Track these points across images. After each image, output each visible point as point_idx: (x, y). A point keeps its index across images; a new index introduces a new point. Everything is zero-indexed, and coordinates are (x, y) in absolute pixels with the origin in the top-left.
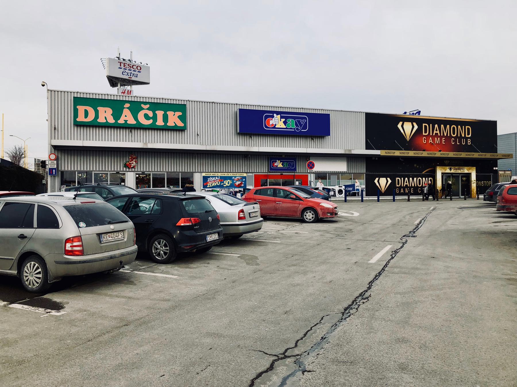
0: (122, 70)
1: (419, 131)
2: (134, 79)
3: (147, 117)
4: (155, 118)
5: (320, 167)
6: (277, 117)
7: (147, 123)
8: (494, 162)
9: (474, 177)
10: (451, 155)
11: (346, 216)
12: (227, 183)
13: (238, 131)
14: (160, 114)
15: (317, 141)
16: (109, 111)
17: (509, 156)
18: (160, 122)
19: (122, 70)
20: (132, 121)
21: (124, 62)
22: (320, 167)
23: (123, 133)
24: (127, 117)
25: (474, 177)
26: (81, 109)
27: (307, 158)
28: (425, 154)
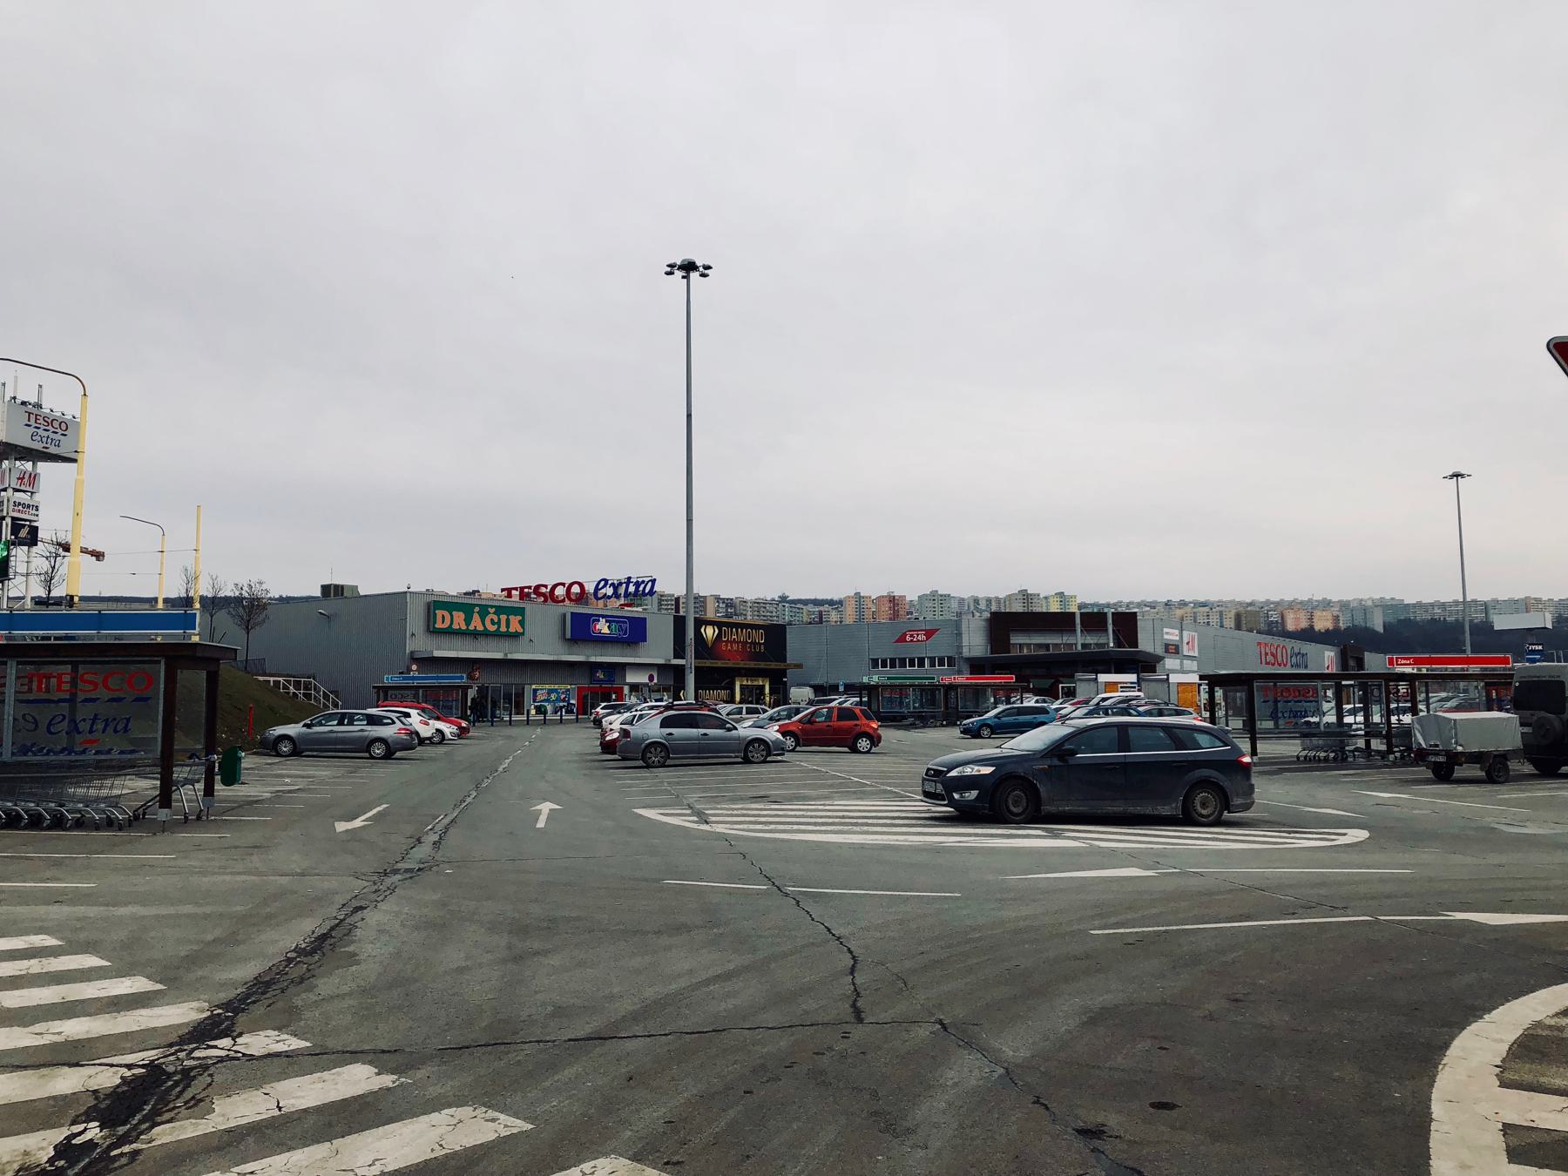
0: (32, 430)
1: (719, 635)
2: (53, 450)
3: (493, 622)
4: (499, 623)
5: (632, 678)
6: (603, 621)
7: (492, 628)
8: (783, 673)
9: (767, 690)
10: (752, 665)
11: (1544, 836)
12: (553, 697)
13: (568, 635)
14: (504, 618)
15: (628, 650)
16: (462, 615)
17: (799, 666)
18: (503, 629)
19: (32, 430)
20: (480, 628)
21: (35, 411)
22: (632, 678)
23: (468, 641)
24: (476, 624)
25: (767, 690)
26: (439, 613)
27: (623, 668)
28: (719, 664)
